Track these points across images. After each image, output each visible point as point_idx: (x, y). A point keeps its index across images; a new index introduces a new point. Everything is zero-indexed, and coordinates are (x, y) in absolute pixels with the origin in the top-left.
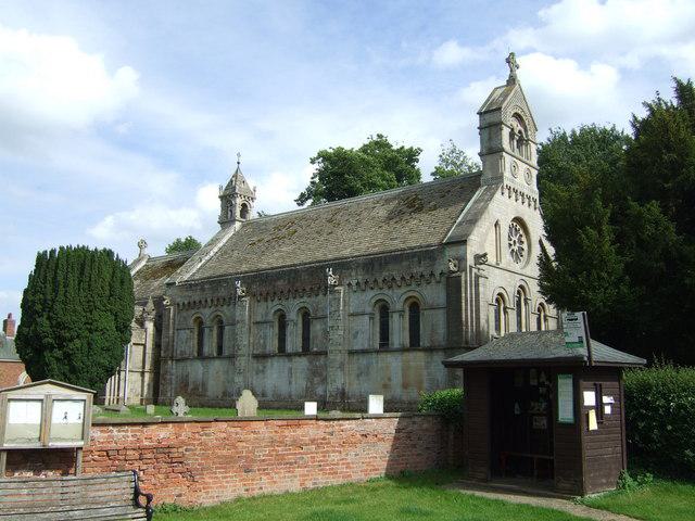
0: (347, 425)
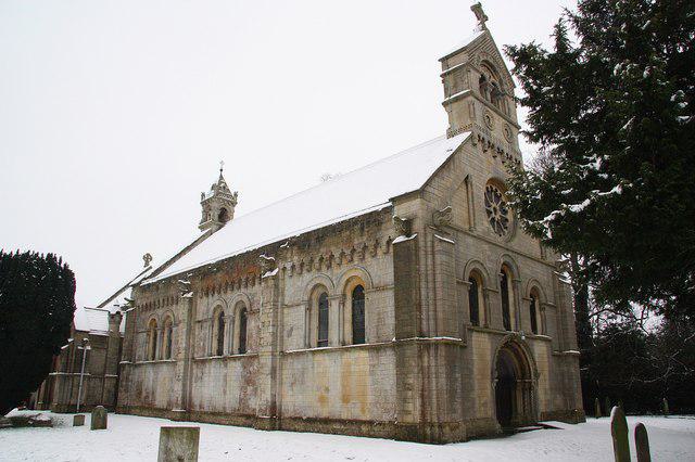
0: (489, 387)
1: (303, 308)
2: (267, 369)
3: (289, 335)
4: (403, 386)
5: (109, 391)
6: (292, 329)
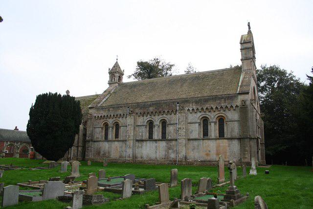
6: (206, 133)
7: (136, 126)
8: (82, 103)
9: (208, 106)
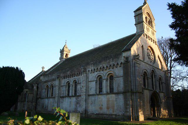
1: (95, 82)
2: (84, 99)
3: (90, 90)
4: (126, 104)
5: (34, 106)
6: (91, 88)
7: (60, 86)
8: (130, 52)
9: (101, 66)
